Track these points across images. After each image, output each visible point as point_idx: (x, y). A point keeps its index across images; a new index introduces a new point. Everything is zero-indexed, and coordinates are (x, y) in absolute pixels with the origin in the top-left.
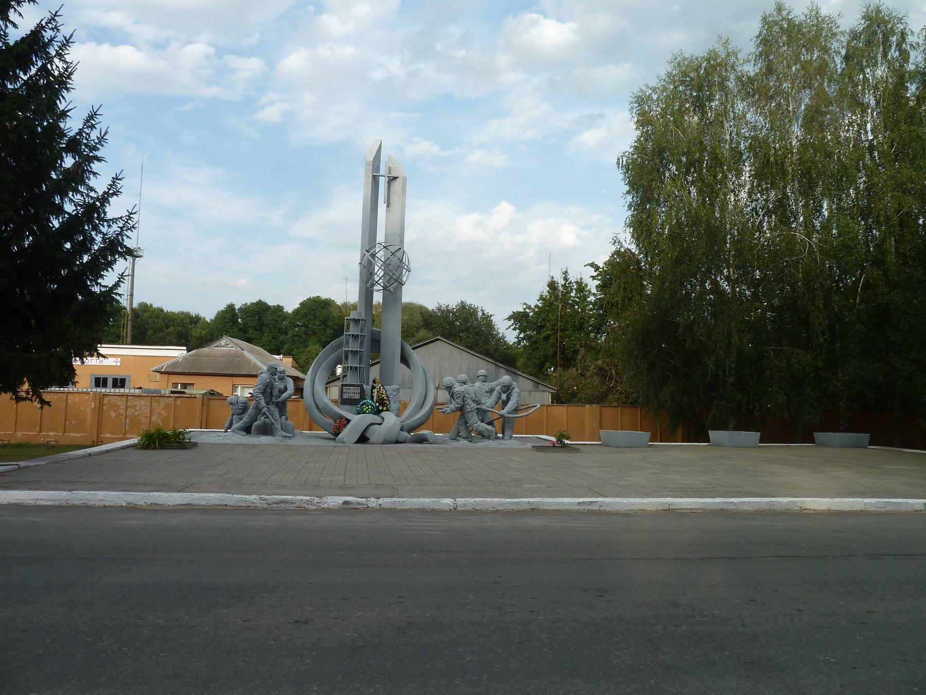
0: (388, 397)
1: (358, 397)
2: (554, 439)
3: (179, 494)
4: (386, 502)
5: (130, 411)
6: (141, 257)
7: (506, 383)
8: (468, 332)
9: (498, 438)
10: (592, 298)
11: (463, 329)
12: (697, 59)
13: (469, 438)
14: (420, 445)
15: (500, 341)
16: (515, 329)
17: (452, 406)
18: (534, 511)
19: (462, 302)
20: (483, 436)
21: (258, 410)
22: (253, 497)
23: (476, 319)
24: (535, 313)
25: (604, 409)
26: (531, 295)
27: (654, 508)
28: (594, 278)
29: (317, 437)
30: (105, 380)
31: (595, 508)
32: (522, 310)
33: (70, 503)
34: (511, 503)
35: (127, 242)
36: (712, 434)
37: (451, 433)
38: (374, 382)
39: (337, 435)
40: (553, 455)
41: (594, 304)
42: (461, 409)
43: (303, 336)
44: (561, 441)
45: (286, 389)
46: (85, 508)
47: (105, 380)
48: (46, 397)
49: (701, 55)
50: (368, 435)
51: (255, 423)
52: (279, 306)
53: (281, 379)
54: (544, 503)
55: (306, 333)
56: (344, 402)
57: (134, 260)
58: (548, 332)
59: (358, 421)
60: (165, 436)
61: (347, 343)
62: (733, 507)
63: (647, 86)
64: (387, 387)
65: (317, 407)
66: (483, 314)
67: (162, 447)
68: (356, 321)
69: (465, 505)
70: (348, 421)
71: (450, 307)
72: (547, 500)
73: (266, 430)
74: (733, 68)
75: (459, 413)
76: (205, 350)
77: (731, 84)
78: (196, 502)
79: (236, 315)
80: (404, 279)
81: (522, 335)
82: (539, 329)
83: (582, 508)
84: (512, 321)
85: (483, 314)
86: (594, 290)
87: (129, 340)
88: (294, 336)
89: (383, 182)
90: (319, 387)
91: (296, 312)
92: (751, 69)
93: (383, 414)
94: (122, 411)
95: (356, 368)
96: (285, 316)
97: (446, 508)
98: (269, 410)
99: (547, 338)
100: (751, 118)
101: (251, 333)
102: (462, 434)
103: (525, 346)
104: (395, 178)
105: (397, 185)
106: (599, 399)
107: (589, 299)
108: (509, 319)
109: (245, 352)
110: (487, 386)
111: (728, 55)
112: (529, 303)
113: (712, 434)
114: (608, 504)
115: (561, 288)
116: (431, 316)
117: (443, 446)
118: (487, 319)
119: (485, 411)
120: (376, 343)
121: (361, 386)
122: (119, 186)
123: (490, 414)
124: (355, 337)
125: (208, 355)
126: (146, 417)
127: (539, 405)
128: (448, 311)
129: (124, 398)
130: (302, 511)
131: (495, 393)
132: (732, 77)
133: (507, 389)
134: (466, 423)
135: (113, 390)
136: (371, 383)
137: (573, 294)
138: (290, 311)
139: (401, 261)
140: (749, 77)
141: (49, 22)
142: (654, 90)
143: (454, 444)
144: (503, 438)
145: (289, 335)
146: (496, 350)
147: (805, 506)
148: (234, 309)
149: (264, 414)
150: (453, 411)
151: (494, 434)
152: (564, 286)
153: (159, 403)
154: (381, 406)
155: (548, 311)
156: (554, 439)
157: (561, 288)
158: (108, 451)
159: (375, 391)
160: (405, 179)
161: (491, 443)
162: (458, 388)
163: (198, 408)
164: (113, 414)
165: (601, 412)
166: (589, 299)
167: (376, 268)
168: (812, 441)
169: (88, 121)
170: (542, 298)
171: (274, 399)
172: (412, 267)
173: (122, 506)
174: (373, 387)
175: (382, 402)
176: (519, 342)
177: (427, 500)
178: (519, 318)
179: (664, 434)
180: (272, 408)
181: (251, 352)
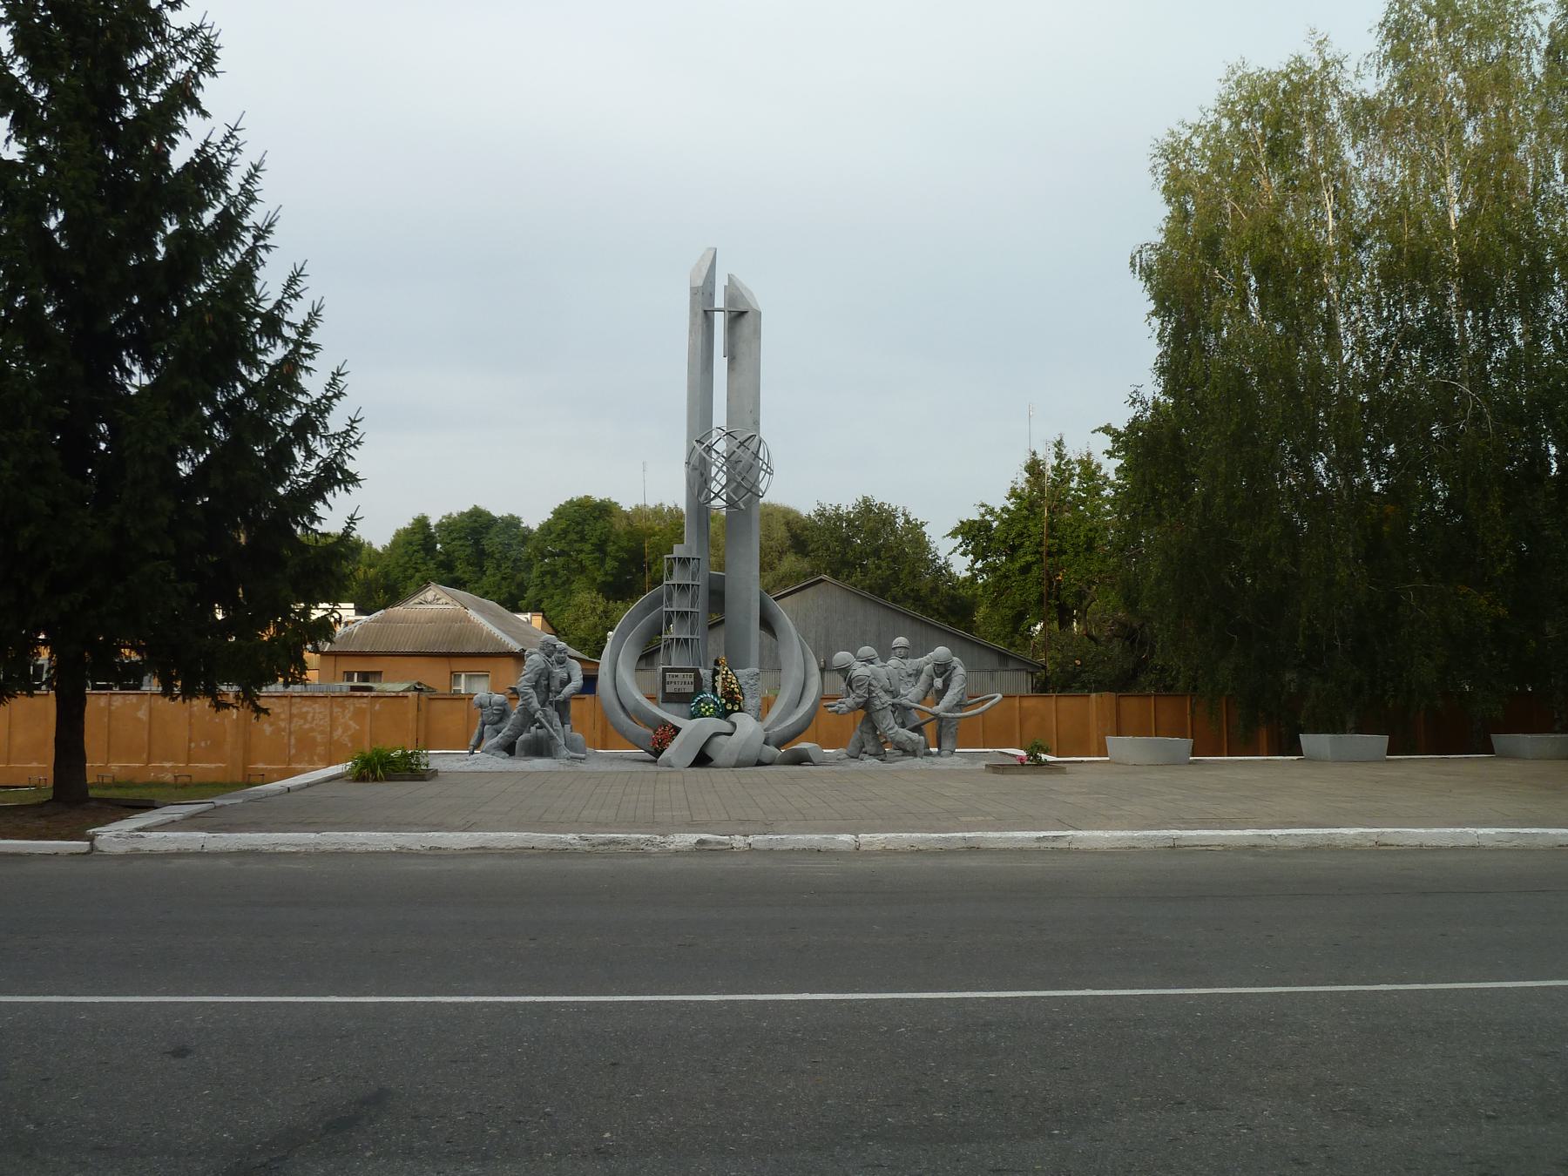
0: (740, 688)
1: (691, 689)
2: (1022, 753)
3: (466, 835)
4: (758, 840)
5: (297, 722)
7: (942, 660)
8: (879, 558)
9: (930, 754)
10: (1108, 492)
11: (863, 558)
12: (1269, 74)
13: (879, 755)
14: (797, 768)
15: (942, 572)
16: (964, 554)
17: (850, 701)
18: (973, 850)
19: (866, 500)
20: (906, 751)
21: (528, 718)
22: (570, 836)
23: (894, 531)
24: (1003, 522)
25: (1125, 702)
26: (992, 486)
27: (1151, 845)
28: (1111, 454)
29: (623, 759)
31: (1063, 845)
32: (978, 518)
33: (321, 848)
34: (937, 840)
35: (350, 466)
36: (1306, 740)
37: (851, 748)
38: (717, 663)
39: (657, 753)
40: (1018, 777)
41: (1113, 502)
42: (866, 705)
43: (561, 572)
44: (1036, 757)
45: (569, 680)
46: (341, 854)
48: (261, 703)
49: (1275, 69)
50: (710, 752)
52: (512, 516)
53: (561, 662)
54: (986, 839)
55: (566, 567)
56: (670, 698)
58: (1029, 558)
59: (693, 730)
60: (392, 762)
61: (670, 599)
62: (1270, 842)
63: (1184, 124)
64: (739, 672)
65: (623, 707)
66: (907, 521)
67: (389, 778)
68: (684, 562)
69: (871, 843)
70: (677, 730)
71: (843, 510)
72: (991, 834)
73: (540, 748)
74: (1334, 84)
75: (862, 713)
76: (398, 610)
77: (1334, 114)
78: (490, 845)
79: (431, 536)
80: (762, 486)
81: (979, 565)
82: (1013, 550)
83: (1044, 845)
84: (960, 539)
85: (907, 521)
86: (1112, 477)
88: (544, 574)
89: (720, 320)
90: (626, 675)
91: (546, 528)
92: (1371, 83)
93: (734, 717)
94: (283, 724)
96: (526, 537)
97: (843, 847)
98: (546, 716)
99: (1026, 569)
100: (1369, 167)
101: (461, 570)
102: (868, 748)
103: (985, 586)
104: (742, 313)
105: (746, 325)
106: (1123, 683)
107: (1104, 493)
108: (954, 534)
109: (470, 612)
110: (912, 664)
111: (1326, 65)
112: (991, 505)
113: (1306, 740)
114: (1081, 840)
115: (1049, 473)
116: (805, 528)
117: (837, 768)
118: (915, 530)
119: (907, 709)
120: (717, 597)
121: (696, 671)
122: (341, 385)
123: (915, 714)
124: (683, 588)
125: (404, 620)
126: (322, 732)
127: (1000, 696)
128: (839, 517)
129: (284, 701)
130: (639, 853)
131: (923, 677)
132: (1334, 102)
133: (943, 669)
134: (875, 729)
136: (712, 665)
137: (1073, 485)
138: (535, 527)
139: (756, 455)
140: (1364, 101)
141: (226, 140)
142: (1197, 130)
143: (855, 765)
144: (939, 754)
145: (535, 572)
146: (934, 590)
147: (1383, 840)
148: (428, 526)
149: (538, 720)
150: (851, 709)
151: (922, 747)
152: (1056, 469)
153: (344, 707)
154: (730, 703)
155: (1027, 518)
156: (1022, 753)
157: (1049, 473)
158: (309, 785)
159: (719, 678)
160: (759, 314)
161: (918, 763)
162: (860, 670)
163: (412, 714)
165: (1118, 705)
166: (1104, 493)
167: (714, 470)
168: (1489, 749)
169: (289, 287)
170: (1013, 493)
172: (775, 465)
173: (391, 852)
174: (716, 673)
175: (731, 696)
176: (974, 577)
177: (817, 837)
178: (973, 534)
179: (1241, 743)
180: (550, 710)
181: (481, 610)
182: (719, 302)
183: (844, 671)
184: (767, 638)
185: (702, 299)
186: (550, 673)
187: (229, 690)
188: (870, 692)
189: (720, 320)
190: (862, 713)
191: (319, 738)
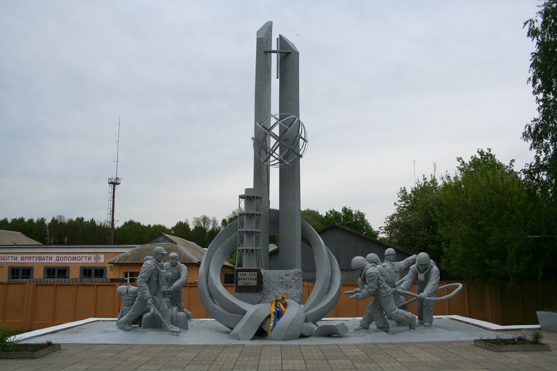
1: (254, 283)
6: (119, 184)
13: (384, 328)
17: (364, 291)
42: (376, 294)
45: (179, 276)
51: (146, 316)
57: (114, 187)
61: (242, 241)
73: (156, 324)
75: (373, 298)
80: (301, 153)
87: (112, 241)
95: (252, 251)
96: (458, 184)
104: (288, 54)
121: (258, 271)
133: (424, 268)
134: (382, 309)
135: (21, 280)
150: (365, 297)
162: (371, 269)
171: (164, 288)
182: (274, 47)
185: (263, 52)
186: (159, 272)
187: (539, 82)
188: (378, 284)
190: (373, 298)
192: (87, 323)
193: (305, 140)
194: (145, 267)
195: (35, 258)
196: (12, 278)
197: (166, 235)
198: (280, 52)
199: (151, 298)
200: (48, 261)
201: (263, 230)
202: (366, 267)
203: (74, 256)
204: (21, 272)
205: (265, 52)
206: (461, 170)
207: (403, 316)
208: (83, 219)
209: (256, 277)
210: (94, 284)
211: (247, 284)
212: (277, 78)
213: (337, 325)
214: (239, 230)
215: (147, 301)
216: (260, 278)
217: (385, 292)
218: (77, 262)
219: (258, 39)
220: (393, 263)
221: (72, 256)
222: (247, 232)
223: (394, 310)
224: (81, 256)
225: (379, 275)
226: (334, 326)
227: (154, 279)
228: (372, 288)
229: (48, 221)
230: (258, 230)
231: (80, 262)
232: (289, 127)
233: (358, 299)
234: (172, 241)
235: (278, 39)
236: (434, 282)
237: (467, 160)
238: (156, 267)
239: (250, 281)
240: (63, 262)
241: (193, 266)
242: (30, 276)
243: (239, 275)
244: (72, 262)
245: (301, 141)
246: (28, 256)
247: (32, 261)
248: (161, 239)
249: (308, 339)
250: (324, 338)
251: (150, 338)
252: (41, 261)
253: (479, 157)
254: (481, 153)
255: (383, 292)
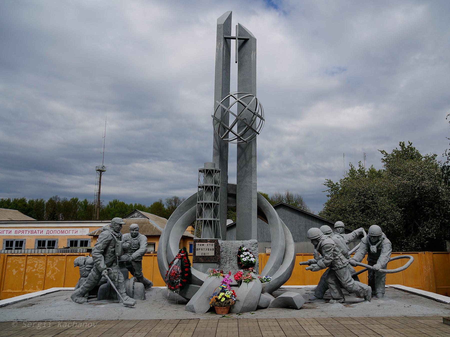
1: (212, 253)
5: (29, 269)
13: (341, 299)
30: (76, 242)
45: (138, 246)
47: (76, 242)
61: (201, 214)
73: (110, 295)
89: (234, 44)
94: (22, 269)
95: (210, 221)
104: (246, 40)
126: (41, 273)
129: (24, 258)
153: (53, 261)
162: (327, 241)
164: (14, 272)
183: (316, 241)
184: (261, 221)
186: (116, 242)
188: (335, 256)
189: (234, 44)
191: (40, 276)
192: (46, 294)
193: (262, 118)
194: (101, 238)
195: (27, 232)
196: (7, 249)
197: (140, 212)
198: (239, 39)
199: (106, 269)
200: (39, 234)
201: (222, 202)
202: (322, 239)
203: (63, 229)
204: (46, 246)
205: (225, 38)
206: (384, 161)
207: (359, 288)
208: (77, 200)
209: (213, 247)
210: (64, 254)
211: (204, 254)
212: (236, 62)
213: (295, 297)
214: (198, 202)
215: (101, 273)
216: (217, 248)
217: (341, 263)
218: (65, 234)
219: (218, 25)
220: (342, 235)
221: (60, 229)
222: (205, 204)
223: (350, 281)
224: (68, 229)
225: (334, 246)
226: (291, 298)
227: (111, 249)
228: (327, 259)
229: (46, 201)
230: (216, 202)
231: (68, 234)
232: (245, 107)
233: (313, 270)
234: (144, 216)
235: (237, 26)
236: (387, 254)
237: (389, 152)
238: (114, 238)
239: (207, 251)
240: (53, 234)
241: (154, 237)
242: (23, 247)
243: (197, 245)
244: (60, 234)
245: (258, 119)
246: (21, 230)
247: (25, 234)
248: (136, 214)
249: (264, 311)
250: (281, 309)
251: (103, 310)
252: (33, 235)
253: (400, 149)
254: (402, 145)
255: (339, 263)
